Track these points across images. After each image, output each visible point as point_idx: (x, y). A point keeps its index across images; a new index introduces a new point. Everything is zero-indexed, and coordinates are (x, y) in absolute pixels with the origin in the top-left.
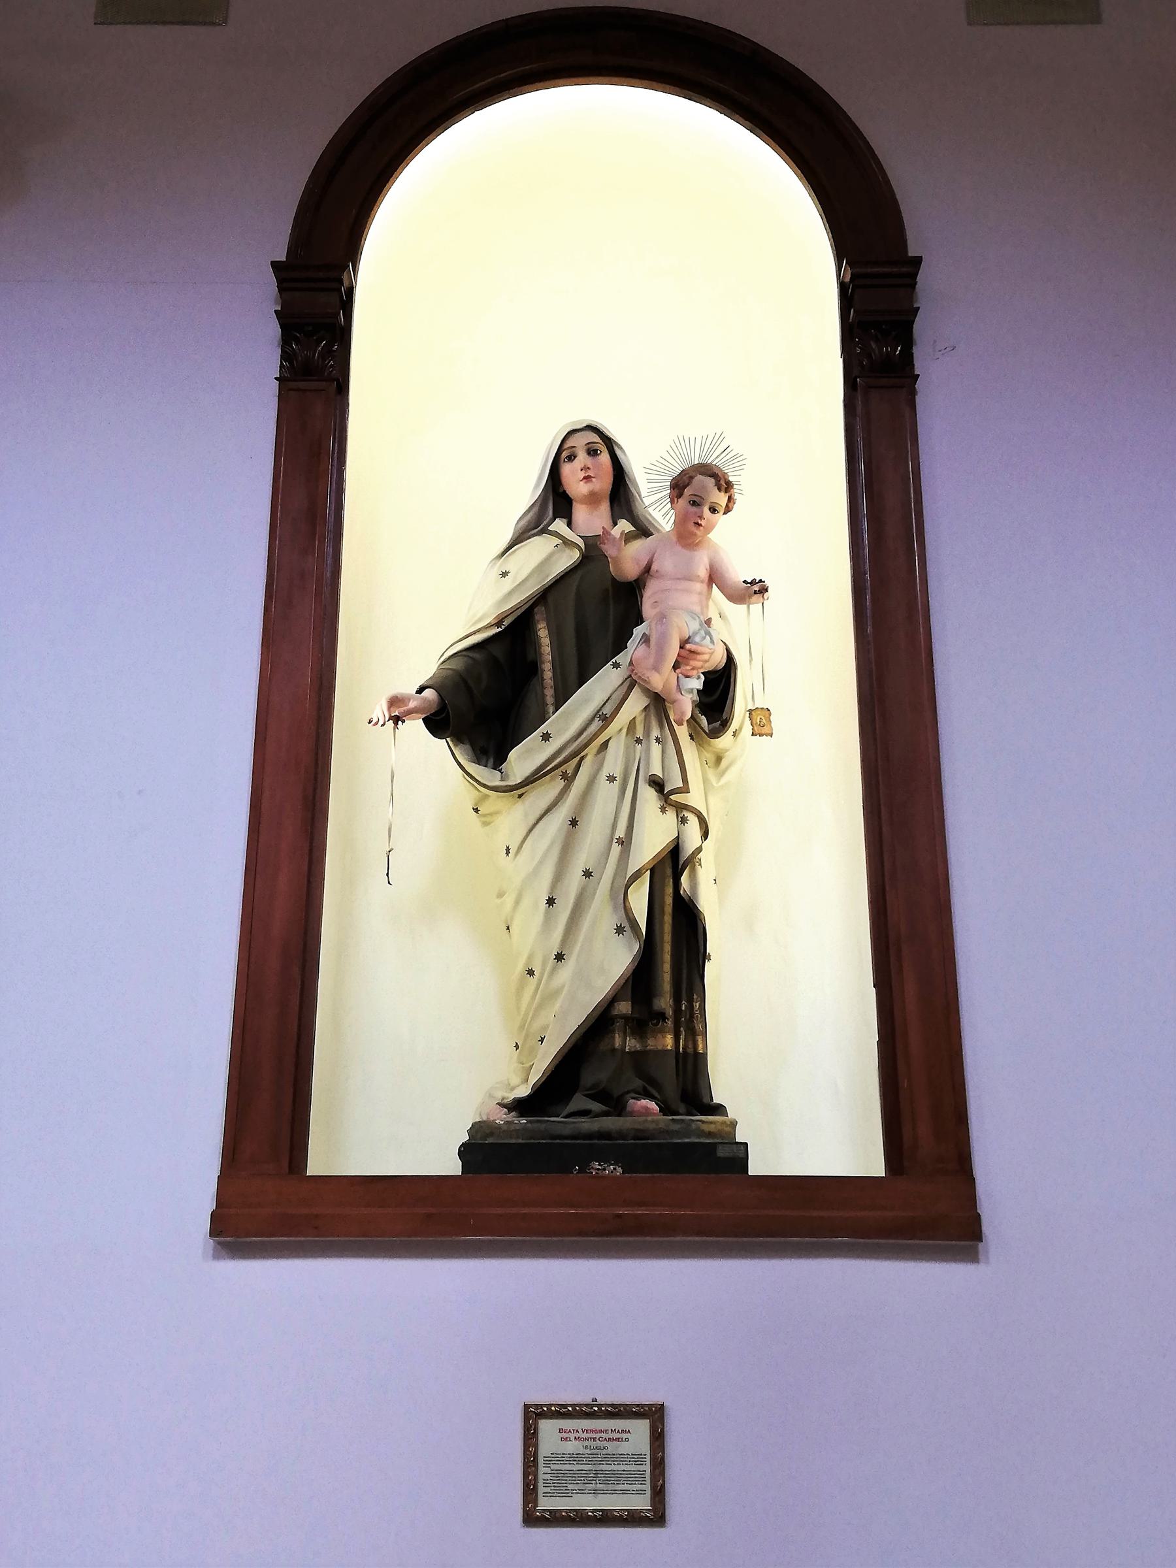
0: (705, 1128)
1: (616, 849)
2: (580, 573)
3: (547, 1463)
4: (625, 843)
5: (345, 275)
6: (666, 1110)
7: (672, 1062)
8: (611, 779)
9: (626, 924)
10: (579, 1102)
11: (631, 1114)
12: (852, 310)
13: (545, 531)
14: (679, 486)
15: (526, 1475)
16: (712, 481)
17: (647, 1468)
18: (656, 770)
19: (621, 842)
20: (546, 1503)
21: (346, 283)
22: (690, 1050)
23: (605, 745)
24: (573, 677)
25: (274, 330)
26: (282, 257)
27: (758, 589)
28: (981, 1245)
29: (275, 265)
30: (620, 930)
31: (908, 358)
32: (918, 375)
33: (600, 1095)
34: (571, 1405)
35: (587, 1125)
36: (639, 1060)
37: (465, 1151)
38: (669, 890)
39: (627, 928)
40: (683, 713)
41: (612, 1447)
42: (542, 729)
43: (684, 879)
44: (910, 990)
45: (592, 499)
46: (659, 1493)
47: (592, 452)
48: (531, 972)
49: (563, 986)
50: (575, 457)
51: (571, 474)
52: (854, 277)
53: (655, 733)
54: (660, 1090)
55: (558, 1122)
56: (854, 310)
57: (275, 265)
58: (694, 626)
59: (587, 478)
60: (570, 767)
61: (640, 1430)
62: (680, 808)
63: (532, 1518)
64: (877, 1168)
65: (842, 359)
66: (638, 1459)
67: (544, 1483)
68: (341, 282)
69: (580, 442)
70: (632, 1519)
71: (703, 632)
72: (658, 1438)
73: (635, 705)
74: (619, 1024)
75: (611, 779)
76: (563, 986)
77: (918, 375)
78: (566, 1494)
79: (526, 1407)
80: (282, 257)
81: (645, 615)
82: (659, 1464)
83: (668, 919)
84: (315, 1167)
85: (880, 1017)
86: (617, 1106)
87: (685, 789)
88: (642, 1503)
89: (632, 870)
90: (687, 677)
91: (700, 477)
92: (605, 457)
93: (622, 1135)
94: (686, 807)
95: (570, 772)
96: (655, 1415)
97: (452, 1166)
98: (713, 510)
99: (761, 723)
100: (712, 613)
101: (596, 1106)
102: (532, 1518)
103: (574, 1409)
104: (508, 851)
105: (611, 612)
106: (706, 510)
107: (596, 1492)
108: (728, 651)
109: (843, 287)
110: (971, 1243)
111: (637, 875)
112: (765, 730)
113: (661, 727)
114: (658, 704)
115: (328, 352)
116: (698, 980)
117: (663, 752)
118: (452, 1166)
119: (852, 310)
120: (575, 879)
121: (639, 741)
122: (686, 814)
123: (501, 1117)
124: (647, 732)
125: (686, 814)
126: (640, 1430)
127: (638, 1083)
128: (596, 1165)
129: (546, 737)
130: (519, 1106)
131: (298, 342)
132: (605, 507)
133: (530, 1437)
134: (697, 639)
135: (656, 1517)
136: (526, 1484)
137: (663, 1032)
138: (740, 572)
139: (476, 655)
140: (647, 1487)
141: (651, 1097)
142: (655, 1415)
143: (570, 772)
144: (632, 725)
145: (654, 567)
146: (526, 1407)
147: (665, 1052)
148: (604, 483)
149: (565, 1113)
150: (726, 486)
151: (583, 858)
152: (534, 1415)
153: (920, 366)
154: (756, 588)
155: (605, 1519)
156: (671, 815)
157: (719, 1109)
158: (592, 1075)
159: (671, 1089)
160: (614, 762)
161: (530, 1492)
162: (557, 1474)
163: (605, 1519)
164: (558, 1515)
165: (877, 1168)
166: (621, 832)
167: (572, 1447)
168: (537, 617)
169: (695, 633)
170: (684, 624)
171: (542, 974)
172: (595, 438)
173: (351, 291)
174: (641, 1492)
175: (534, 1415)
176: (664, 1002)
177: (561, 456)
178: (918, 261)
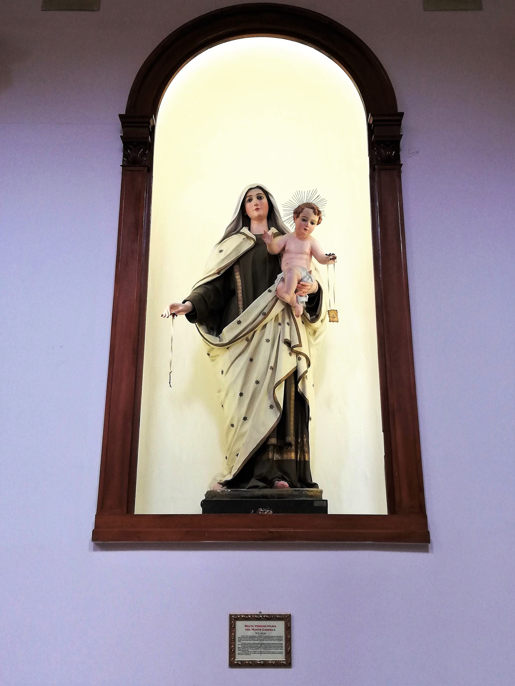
0: (309, 493)
1: (270, 371)
2: (254, 251)
3: (240, 640)
4: (274, 369)
5: (151, 120)
6: (291, 485)
7: (294, 465)
8: (268, 341)
9: (274, 404)
10: (254, 482)
11: (277, 487)
12: (373, 136)
13: (239, 232)
14: (297, 212)
15: (230, 645)
16: (312, 210)
17: (283, 642)
18: (287, 337)
19: (272, 368)
20: (239, 658)
21: (152, 124)
22: (302, 459)
23: (265, 326)
24: (251, 296)
25: (120, 144)
26: (124, 113)
27: (332, 258)
28: (429, 545)
29: (121, 116)
30: (271, 407)
31: (397, 157)
32: (402, 164)
33: (263, 479)
34: (250, 615)
35: (257, 492)
36: (280, 464)
37: (204, 504)
38: (293, 389)
39: (275, 406)
40: (299, 312)
41: (268, 633)
42: (238, 319)
43: (300, 385)
44: (399, 433)
45: (259, 218)
46: (288, 653)
47: (259, 198)
48: (232, 425)
49: (247, 431)
50: (252, 200)
51: (250, 207)
52: (374, 121)
53: (287, 321)
54: (289, 477)
55: (244, 491)
56: (374, 136)
57: (121, 116)
58: (304, 274)
59: (257, 209)
60: (250, 336)
61: (280, 626)
62: (298, 353)
63: (233, 664)
64: (384, 511)
65: (369, 157)
66: (279, 638)
67: (238, 649)
68: (149, 123)
69: (254, 193)
70: (277, 665)
71: (308, 277)
72: (288, 629)
73: (278, 308)
74: (271, 448)
75: (268, 341)
76: (247, 431)
77: (402, 164)
78: (248, 654)
79: (231, 615)
80: (124, 113)
81: (282, 269)
82: (288, 641)
83: (292, 402)
84: (138, 511)
85: (385, 445)
86: (270, 484)
87: (300, 345)
88: (281, 657)
89: (277, 381)
90: (301, 296)
91: (306, 209)
92: (265, 200)
93: (272, 497)
94: (300, 353)
95: (250, 338)
96: (287, 619)
97: (198, 510)
98: (312, 223)
99: (333, 316)
100: (312, 268)
101: (261, 484)
102: (233, 664)
103: (251, 616)
104: (222, 372)
105: (268, 268)
106: (309, 223)
107: (261, 653)
108: (319, 285)
109: (369, 126)
110: (425, 544)
111: (279, 383)
112: (335, 319)
113: (290, 318)
114: (288, 308)
115: (144, 154)
116: (305, 429)
117: (290, 329)
118: (198, 510)
119: (373, 136)
120: (252, 385)
121: (280, 324)
122: (301, 356)
123: (219, 489)
124: (283, 320)
125: (301, 356)
126: (280, 626)
127: (279, 474)
128: (261, 510)
129: (239, 322)
130: (227, 484)
131: (130, 150)
132: (265, 222)
133: (232, 629)
134: (305, 280)
135: (287, 664)
136: (230, 649)
137: (290, 451)
138: (324, 250)
139: (209, 287)
140: (283, 651)
141: (285, 480)
142: (287, 619)
143: (250, 338)
144: (277, 317)
145: (287, 248)
146: (231, 615)
147: (291, 460)
148: (264, 211)
149: (247, 487)
150: (318, 213)
151: (255, 376)
152: (234, 619)
153: (403, 160)
154: (331, 257)
155: (265, 665)
156: (294, 357)
157: (315, 485)
158: (259, 470)
159: (294, 477)
160: (269, 333)
161: (232, 653)
162: (244, 645)
163: (265, 665)
164: (244, 663)
165: (384, 511)
166: (272, 364)
167: (251, 633)
168: (235, 270)
169: (304, 277)
170: (299, 273)
171: (237, 426)
172: (261, 192)
173: (154, 127)
174: (281, 653)
175: (234, 619)
176: (291, 439)
177: (246, 200)
178: (402, 114)
